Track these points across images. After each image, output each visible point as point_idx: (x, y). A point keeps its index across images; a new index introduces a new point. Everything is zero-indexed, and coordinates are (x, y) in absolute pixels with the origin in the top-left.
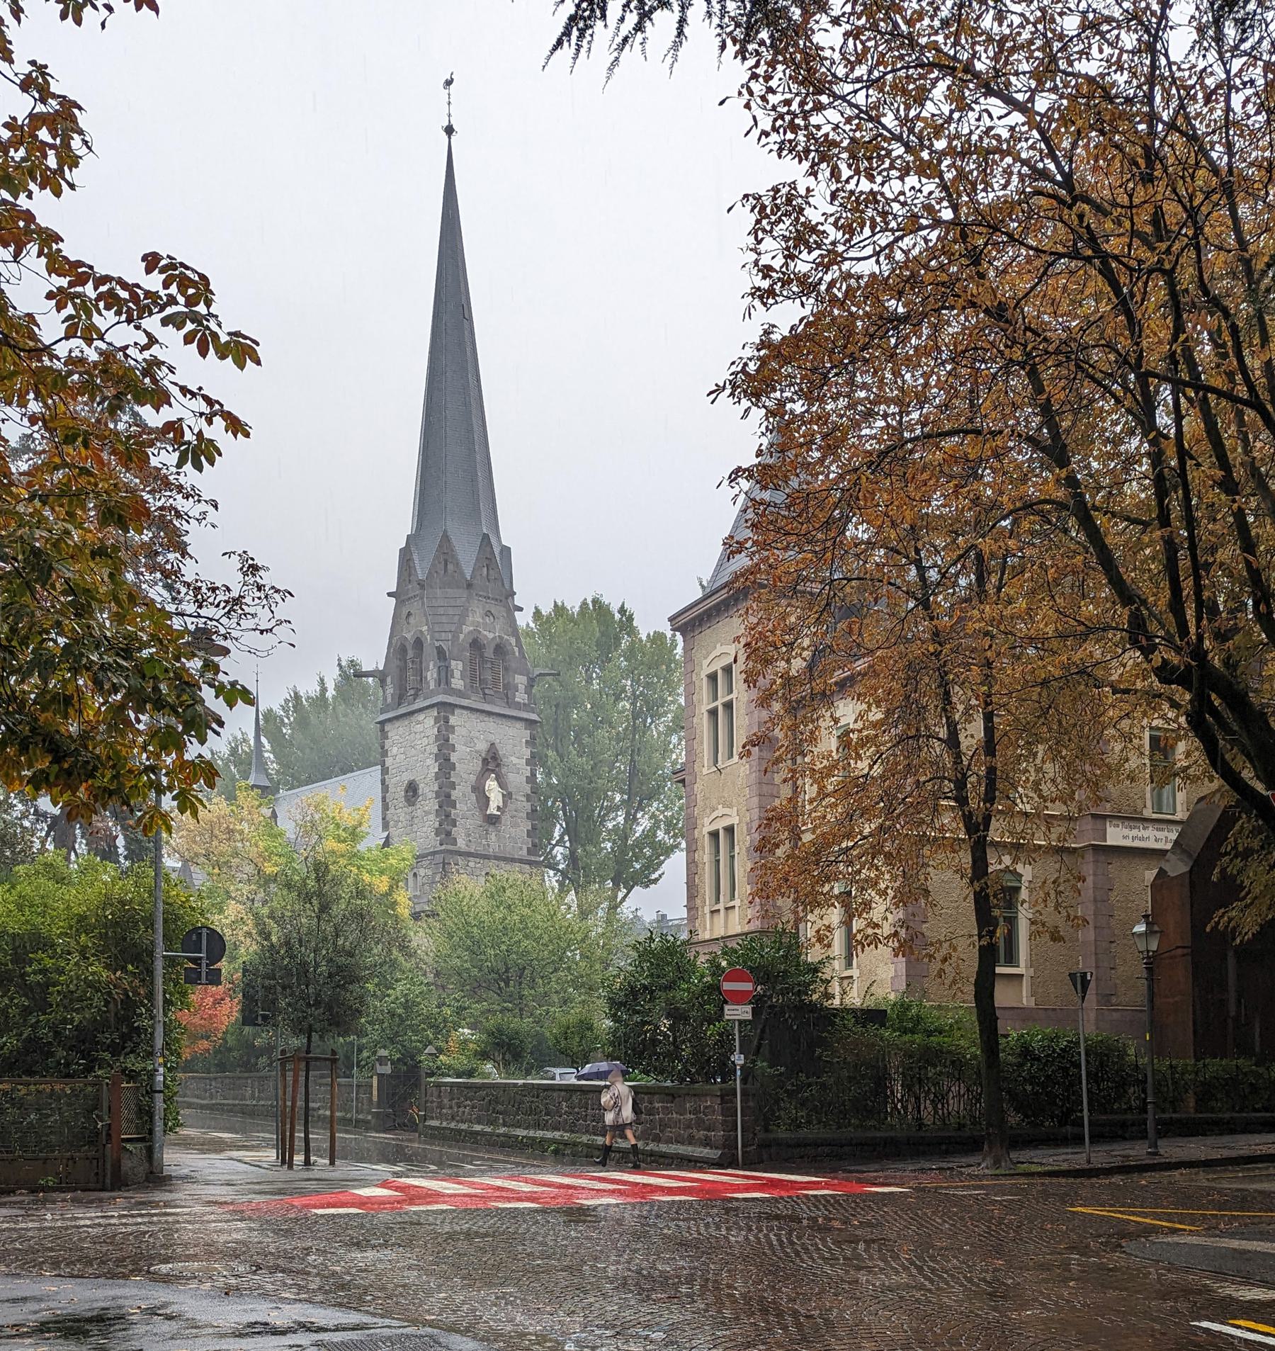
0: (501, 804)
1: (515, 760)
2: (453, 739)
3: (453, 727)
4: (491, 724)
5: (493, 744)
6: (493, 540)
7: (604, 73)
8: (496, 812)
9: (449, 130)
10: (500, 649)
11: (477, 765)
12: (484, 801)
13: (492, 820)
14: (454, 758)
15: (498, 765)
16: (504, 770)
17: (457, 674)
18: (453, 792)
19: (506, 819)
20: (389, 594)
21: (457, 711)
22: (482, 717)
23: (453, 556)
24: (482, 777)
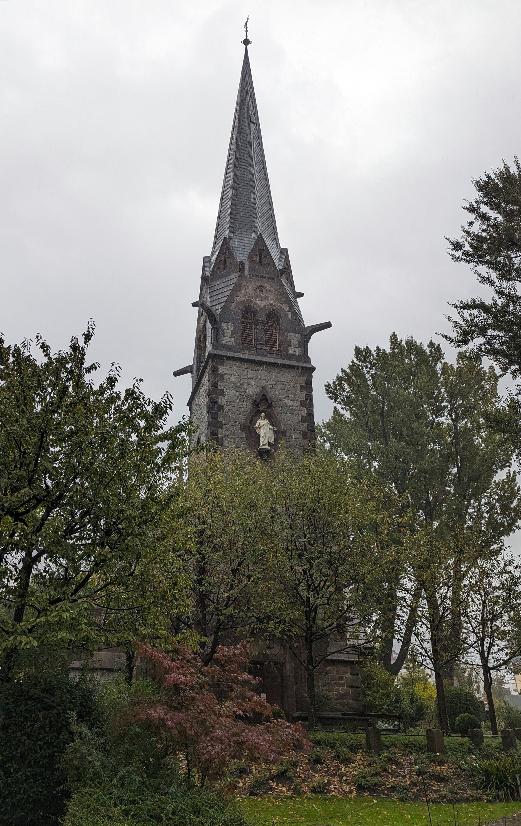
0: (272, 441)
1: (288, 402)
2: (221, 385)
3: (222, 375)
4: (262, 373)
5: (263, 387)
6: (269, 243)
7: (468, 300)
8: (267, 447)
9: (246, 42)
10: (273, 316)
11: (248, 407)
12: (253, 437)
13: (264, 455)
14: (222, 401)
15: (270, 406)
16: (276, 411)
17: (228, 333)
18: (220, 431)
19: (280, 455)
20: (194, 305)
21: (227, 362)
22: (253, 366)
23: (231, 253)
24: (255, 416)
